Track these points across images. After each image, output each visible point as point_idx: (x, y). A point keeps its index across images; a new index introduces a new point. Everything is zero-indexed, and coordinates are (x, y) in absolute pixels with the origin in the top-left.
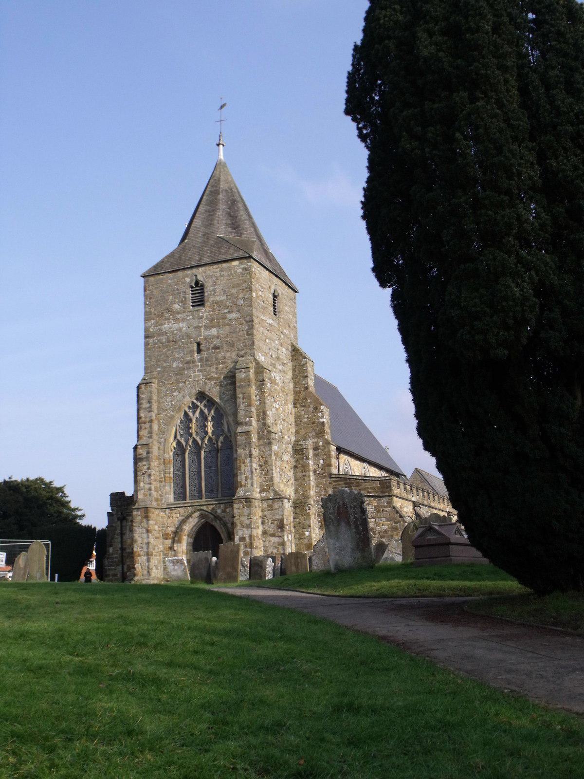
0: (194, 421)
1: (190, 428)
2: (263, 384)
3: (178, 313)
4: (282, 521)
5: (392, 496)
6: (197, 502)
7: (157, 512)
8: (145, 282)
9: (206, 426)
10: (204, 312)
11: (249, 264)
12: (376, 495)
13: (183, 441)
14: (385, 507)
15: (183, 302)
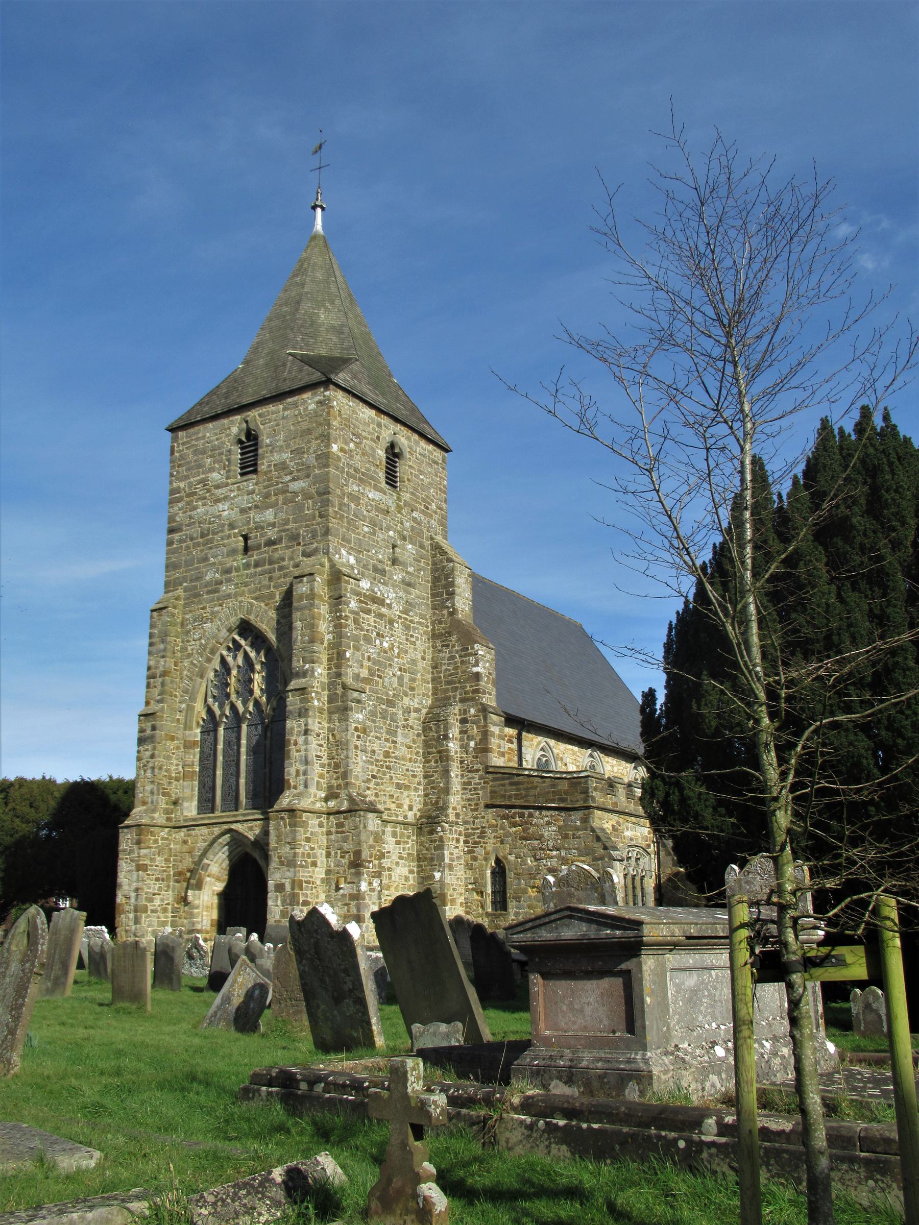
0: (234, 672)
1: (228, 685)
2: (340, 604)
3: (218, 487)
4: (358, 853)
5: (588, 808)
6: (228, 816)
7: (164, 833)
8: (175, 439)
9: (251, 681)
10: (251, 483)
11: (327, 393)
12: (562, 805)
13: (216, 708)
14: (577, 829)
15: (227, 468)
